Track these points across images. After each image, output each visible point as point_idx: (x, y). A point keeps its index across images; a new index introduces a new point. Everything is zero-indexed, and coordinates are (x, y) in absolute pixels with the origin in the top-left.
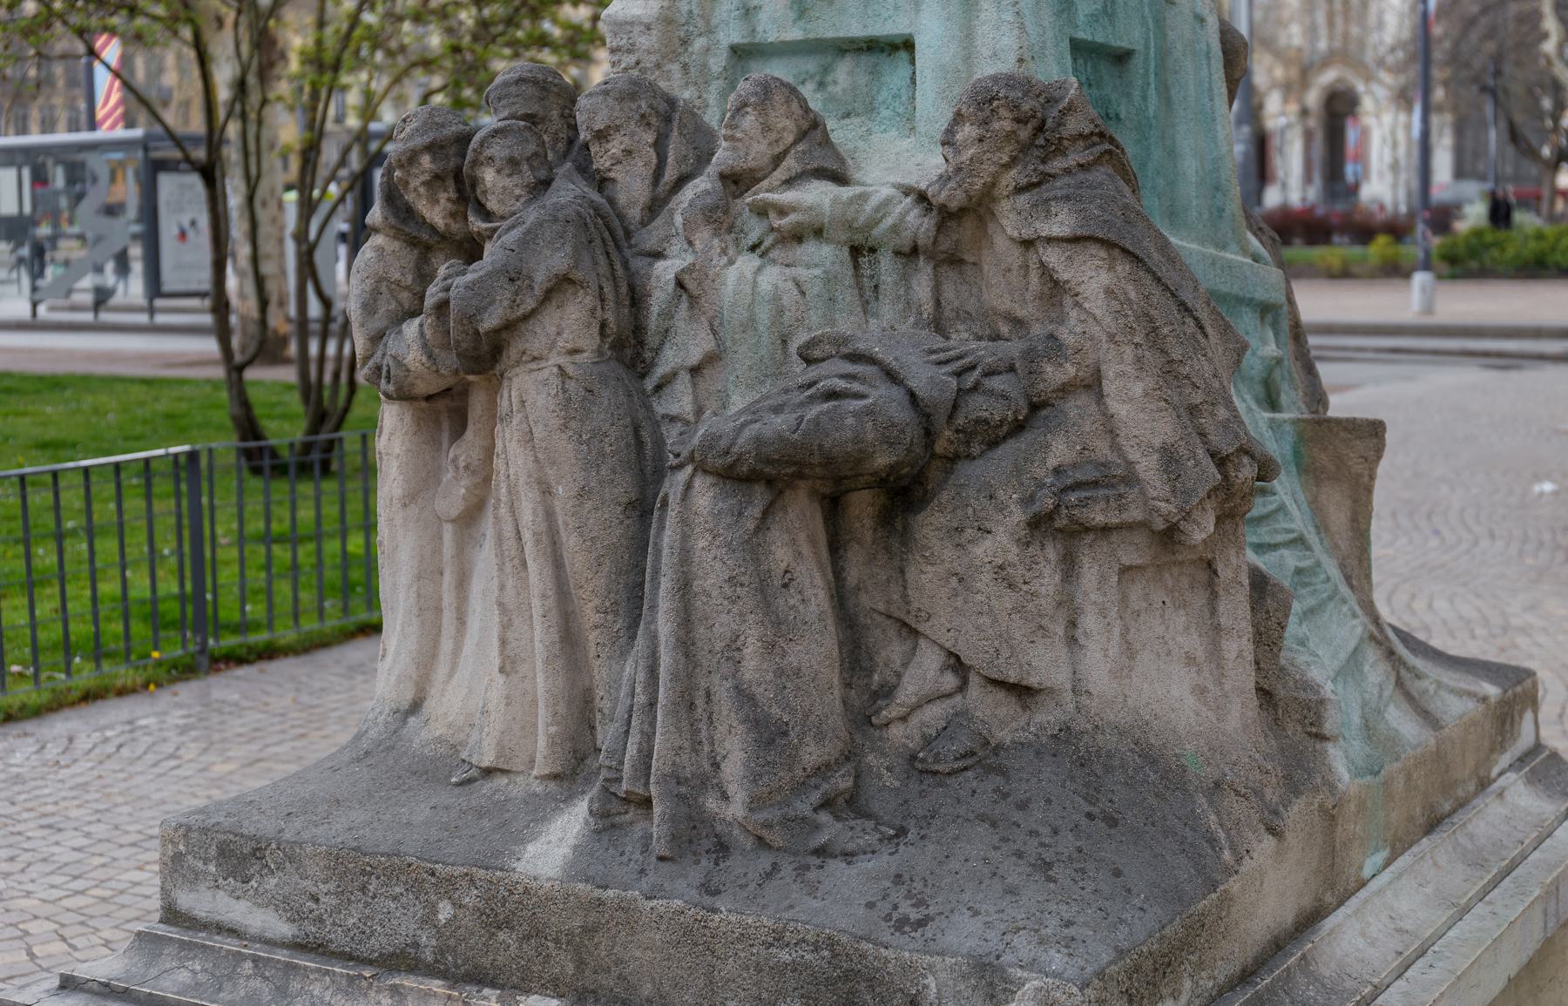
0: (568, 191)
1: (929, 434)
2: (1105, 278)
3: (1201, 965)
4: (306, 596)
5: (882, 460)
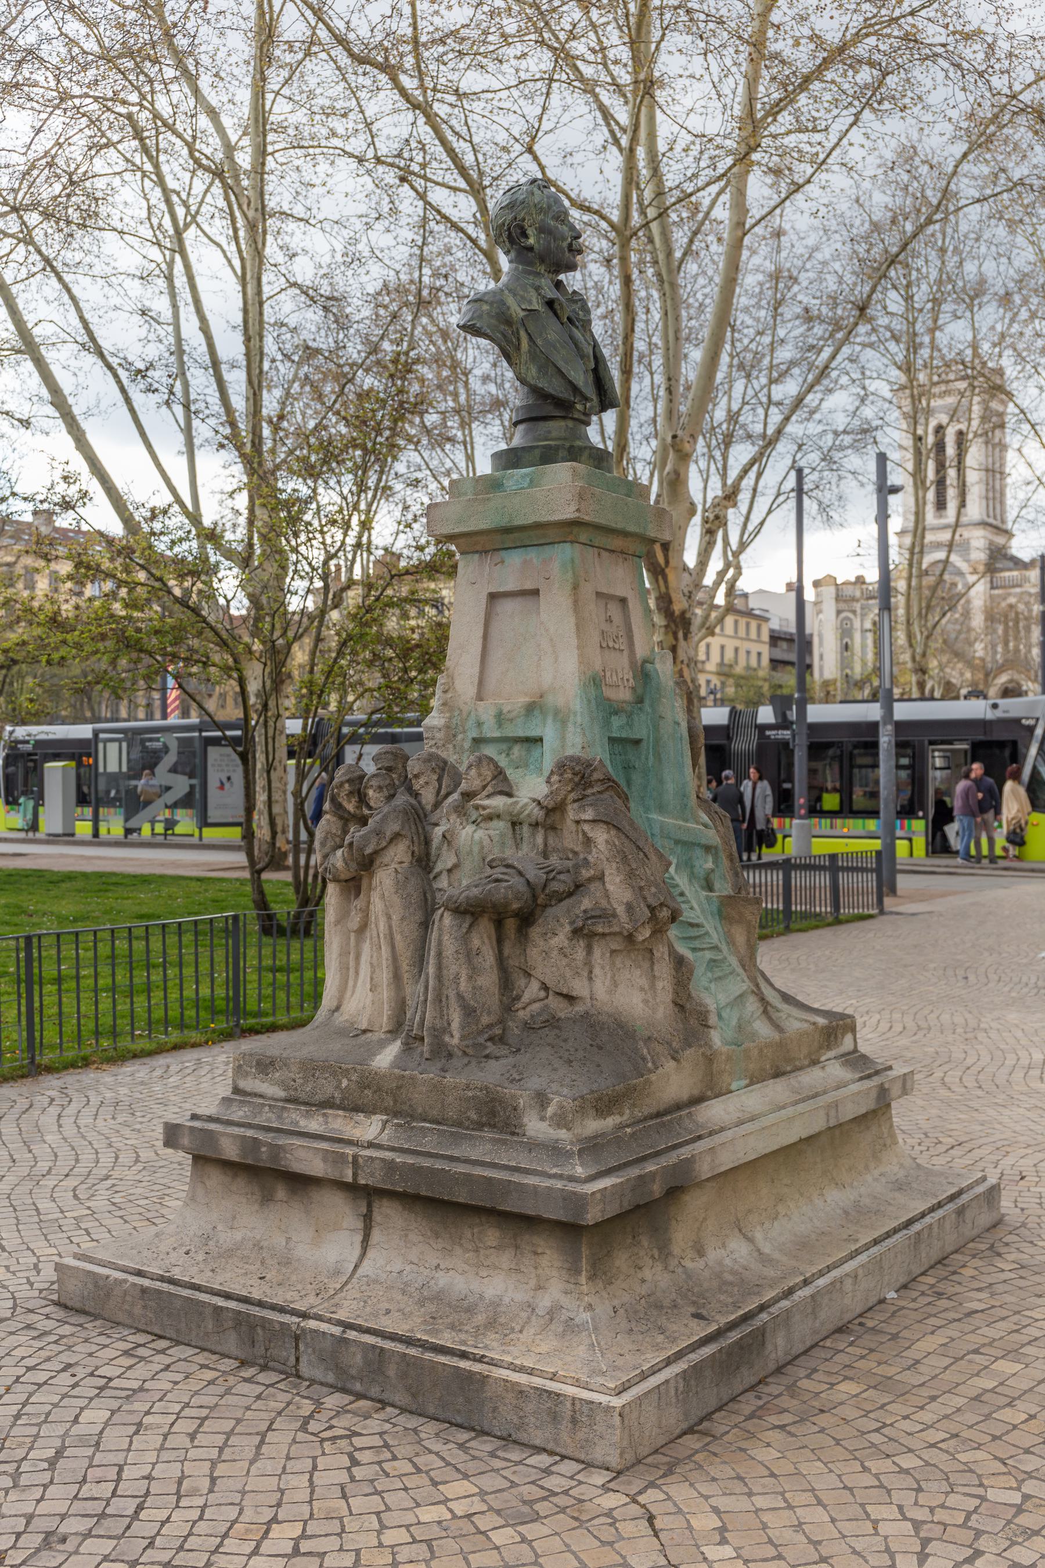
0: (402, 799)
1: (535, 897)
2: (605, 836)
3: (634, 1105)
4: (293, 1000)
5: (515, 906)
